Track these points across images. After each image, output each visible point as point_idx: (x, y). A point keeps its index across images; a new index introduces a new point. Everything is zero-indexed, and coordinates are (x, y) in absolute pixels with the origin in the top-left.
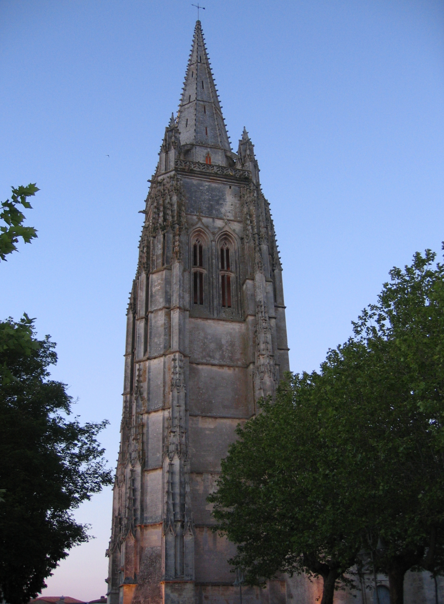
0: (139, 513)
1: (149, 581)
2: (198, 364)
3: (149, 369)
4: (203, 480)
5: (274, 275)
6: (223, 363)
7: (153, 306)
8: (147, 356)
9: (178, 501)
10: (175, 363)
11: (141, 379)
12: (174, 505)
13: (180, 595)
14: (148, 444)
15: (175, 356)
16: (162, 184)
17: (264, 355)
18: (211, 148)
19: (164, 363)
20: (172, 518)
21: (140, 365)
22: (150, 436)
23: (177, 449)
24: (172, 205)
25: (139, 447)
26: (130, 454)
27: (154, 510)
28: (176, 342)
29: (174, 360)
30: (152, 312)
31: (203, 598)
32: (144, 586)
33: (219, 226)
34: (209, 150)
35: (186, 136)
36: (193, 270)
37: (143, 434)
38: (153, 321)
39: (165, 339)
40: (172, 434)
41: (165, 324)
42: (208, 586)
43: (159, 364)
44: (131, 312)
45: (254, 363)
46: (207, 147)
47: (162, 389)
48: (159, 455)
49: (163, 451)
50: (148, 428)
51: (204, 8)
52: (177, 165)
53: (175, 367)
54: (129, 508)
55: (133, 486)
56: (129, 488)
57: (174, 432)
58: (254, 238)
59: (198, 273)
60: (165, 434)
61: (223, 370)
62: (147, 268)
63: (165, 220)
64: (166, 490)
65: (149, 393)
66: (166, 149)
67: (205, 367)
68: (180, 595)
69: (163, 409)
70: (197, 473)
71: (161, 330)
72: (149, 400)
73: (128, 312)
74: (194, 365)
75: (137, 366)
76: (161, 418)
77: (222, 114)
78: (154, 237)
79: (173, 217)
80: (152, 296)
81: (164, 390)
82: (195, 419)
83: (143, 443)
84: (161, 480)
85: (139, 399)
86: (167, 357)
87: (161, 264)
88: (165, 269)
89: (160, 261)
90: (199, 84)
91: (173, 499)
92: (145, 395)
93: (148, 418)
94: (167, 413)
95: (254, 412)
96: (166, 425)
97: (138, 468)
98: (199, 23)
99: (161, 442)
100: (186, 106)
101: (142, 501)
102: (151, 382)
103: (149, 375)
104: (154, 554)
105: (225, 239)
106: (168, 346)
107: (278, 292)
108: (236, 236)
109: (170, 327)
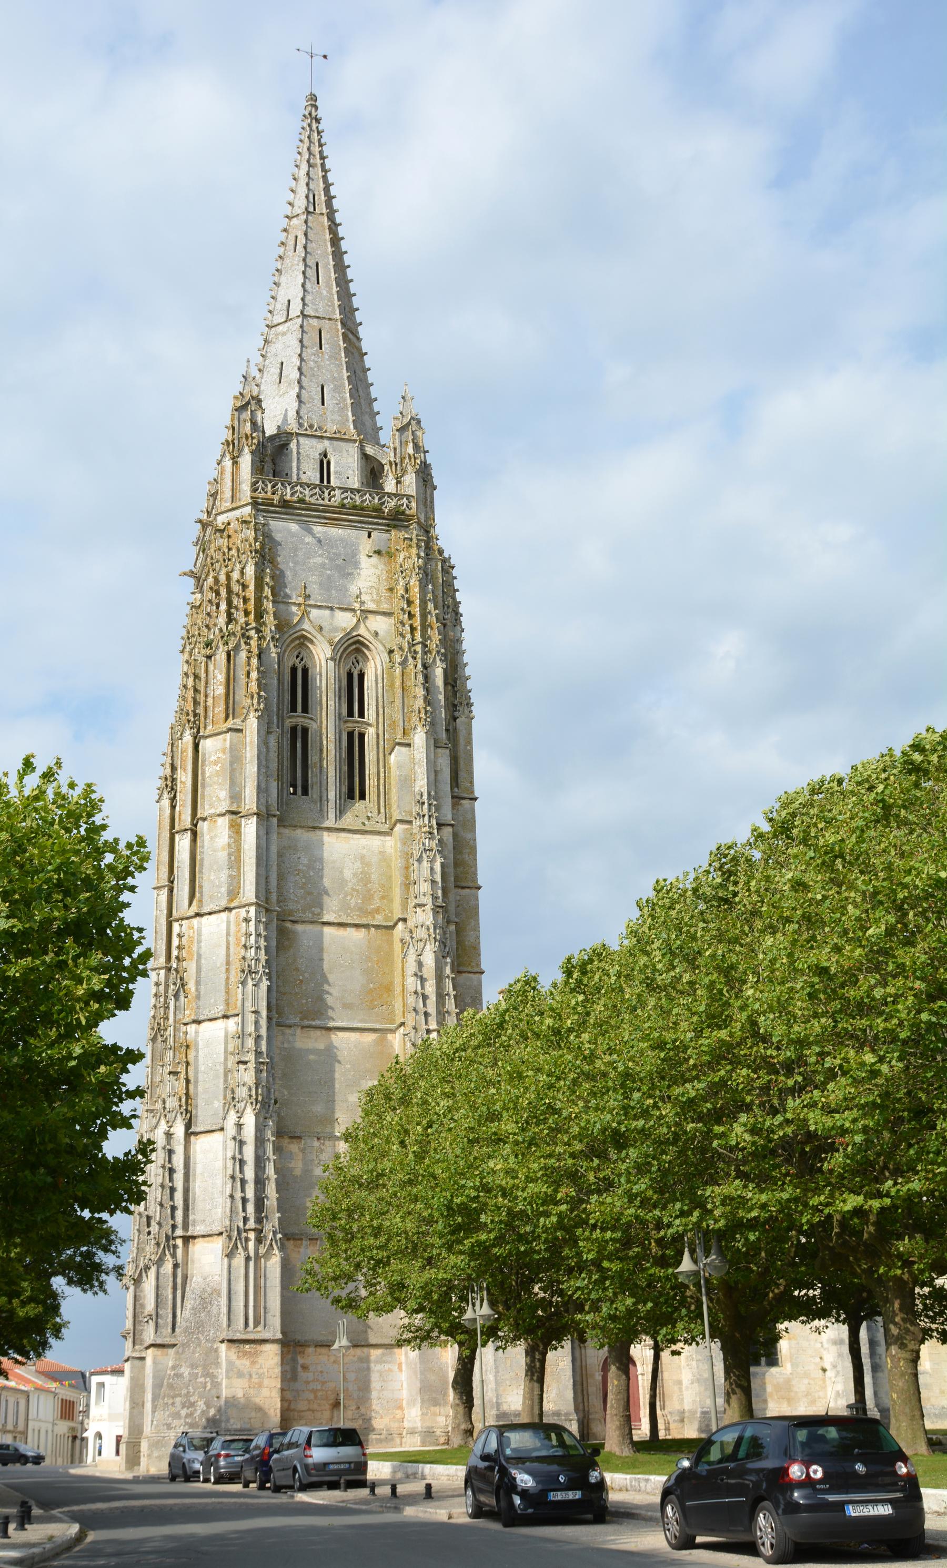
0: (179, 1214)
1: (198, 1338)
2: (294, 922)
3: (199, 935)
4: (303, 1150)
5: (455, 729)
6: (344, 920)
7: (207, 807)
8: (194, 909)
9: (250, 1193)
11: (184, 953)
12: (244, 1200)
13: (253, 1363)
14: (196, 1082)
15: (248, 912)
17: (424, 905)
18: (330, 439)
19: (228, 923)
20: (241, 1224)
22: (202, 1068)
23: (250, 1096)
24: (245, 587)
25: (180, 1086)
26: (164, 1102)
27: (208, 1207)
29: (247, 920)
30: (204, 819)
31: (300, 1369)
32: (189, 1346)
33: (344, 625)
34: (326, 443)
35: (277, 412)
36: (288, 723)
37: (188, 1064)
38: (207, 838)
39: (230, 876)
40: (242, 1067)
41: (229, 845)
42: (309, 1346)
43: (218, 925)
44: (166, 795)
46: (322, 437)
47: (224, 976)
48: (218, 1104)
49: (225, 1098)
50: (197, 1051)
51: (325, 57)
52: (255, 490)
54: (161, 1205)
55: (170, 1162)
56: (163, 1167)
57: (246, 1063)
58: (416, 652)
59: (299, 728)
60: (230, 1066)
62: (194, 722)
63: (230, 619)
64: (230, 1172)
65: (198, 983)
66: (233, 448)
68: (253, 1363)
69: (226, 1017)
70: (291, 1138)
71: (223, 855)
72: (198, 997)
73: (161, 796)
74: (288, 925)
75: (176, 927)
76: (222, 1034)
77: (359, 340)
78: (209, 657)
79: (247, 614)
81: (228, 978)
82: (288, 1031)
83: (188, 1081)
84: (221, 1153)
85: (182, 993)
86: (234, 912)
87: (223, 716)
88: (230, 730)
89: (220, 709)
90: (309, 271)
91: (243, 1190)
92: (191, 986)
93: (197, 1032)
94: (232, 1025)
95: (402, 1020)
96: (231, 1048)
97: (179, 1130)
98: (313, 98)
99: (222, 1080)
100: (281, 328)
101: (186, 1191)
103: (199, 948)
104: (209, 1290)
106: (233, 893)
108: (381, 647)
109: (239, 851)
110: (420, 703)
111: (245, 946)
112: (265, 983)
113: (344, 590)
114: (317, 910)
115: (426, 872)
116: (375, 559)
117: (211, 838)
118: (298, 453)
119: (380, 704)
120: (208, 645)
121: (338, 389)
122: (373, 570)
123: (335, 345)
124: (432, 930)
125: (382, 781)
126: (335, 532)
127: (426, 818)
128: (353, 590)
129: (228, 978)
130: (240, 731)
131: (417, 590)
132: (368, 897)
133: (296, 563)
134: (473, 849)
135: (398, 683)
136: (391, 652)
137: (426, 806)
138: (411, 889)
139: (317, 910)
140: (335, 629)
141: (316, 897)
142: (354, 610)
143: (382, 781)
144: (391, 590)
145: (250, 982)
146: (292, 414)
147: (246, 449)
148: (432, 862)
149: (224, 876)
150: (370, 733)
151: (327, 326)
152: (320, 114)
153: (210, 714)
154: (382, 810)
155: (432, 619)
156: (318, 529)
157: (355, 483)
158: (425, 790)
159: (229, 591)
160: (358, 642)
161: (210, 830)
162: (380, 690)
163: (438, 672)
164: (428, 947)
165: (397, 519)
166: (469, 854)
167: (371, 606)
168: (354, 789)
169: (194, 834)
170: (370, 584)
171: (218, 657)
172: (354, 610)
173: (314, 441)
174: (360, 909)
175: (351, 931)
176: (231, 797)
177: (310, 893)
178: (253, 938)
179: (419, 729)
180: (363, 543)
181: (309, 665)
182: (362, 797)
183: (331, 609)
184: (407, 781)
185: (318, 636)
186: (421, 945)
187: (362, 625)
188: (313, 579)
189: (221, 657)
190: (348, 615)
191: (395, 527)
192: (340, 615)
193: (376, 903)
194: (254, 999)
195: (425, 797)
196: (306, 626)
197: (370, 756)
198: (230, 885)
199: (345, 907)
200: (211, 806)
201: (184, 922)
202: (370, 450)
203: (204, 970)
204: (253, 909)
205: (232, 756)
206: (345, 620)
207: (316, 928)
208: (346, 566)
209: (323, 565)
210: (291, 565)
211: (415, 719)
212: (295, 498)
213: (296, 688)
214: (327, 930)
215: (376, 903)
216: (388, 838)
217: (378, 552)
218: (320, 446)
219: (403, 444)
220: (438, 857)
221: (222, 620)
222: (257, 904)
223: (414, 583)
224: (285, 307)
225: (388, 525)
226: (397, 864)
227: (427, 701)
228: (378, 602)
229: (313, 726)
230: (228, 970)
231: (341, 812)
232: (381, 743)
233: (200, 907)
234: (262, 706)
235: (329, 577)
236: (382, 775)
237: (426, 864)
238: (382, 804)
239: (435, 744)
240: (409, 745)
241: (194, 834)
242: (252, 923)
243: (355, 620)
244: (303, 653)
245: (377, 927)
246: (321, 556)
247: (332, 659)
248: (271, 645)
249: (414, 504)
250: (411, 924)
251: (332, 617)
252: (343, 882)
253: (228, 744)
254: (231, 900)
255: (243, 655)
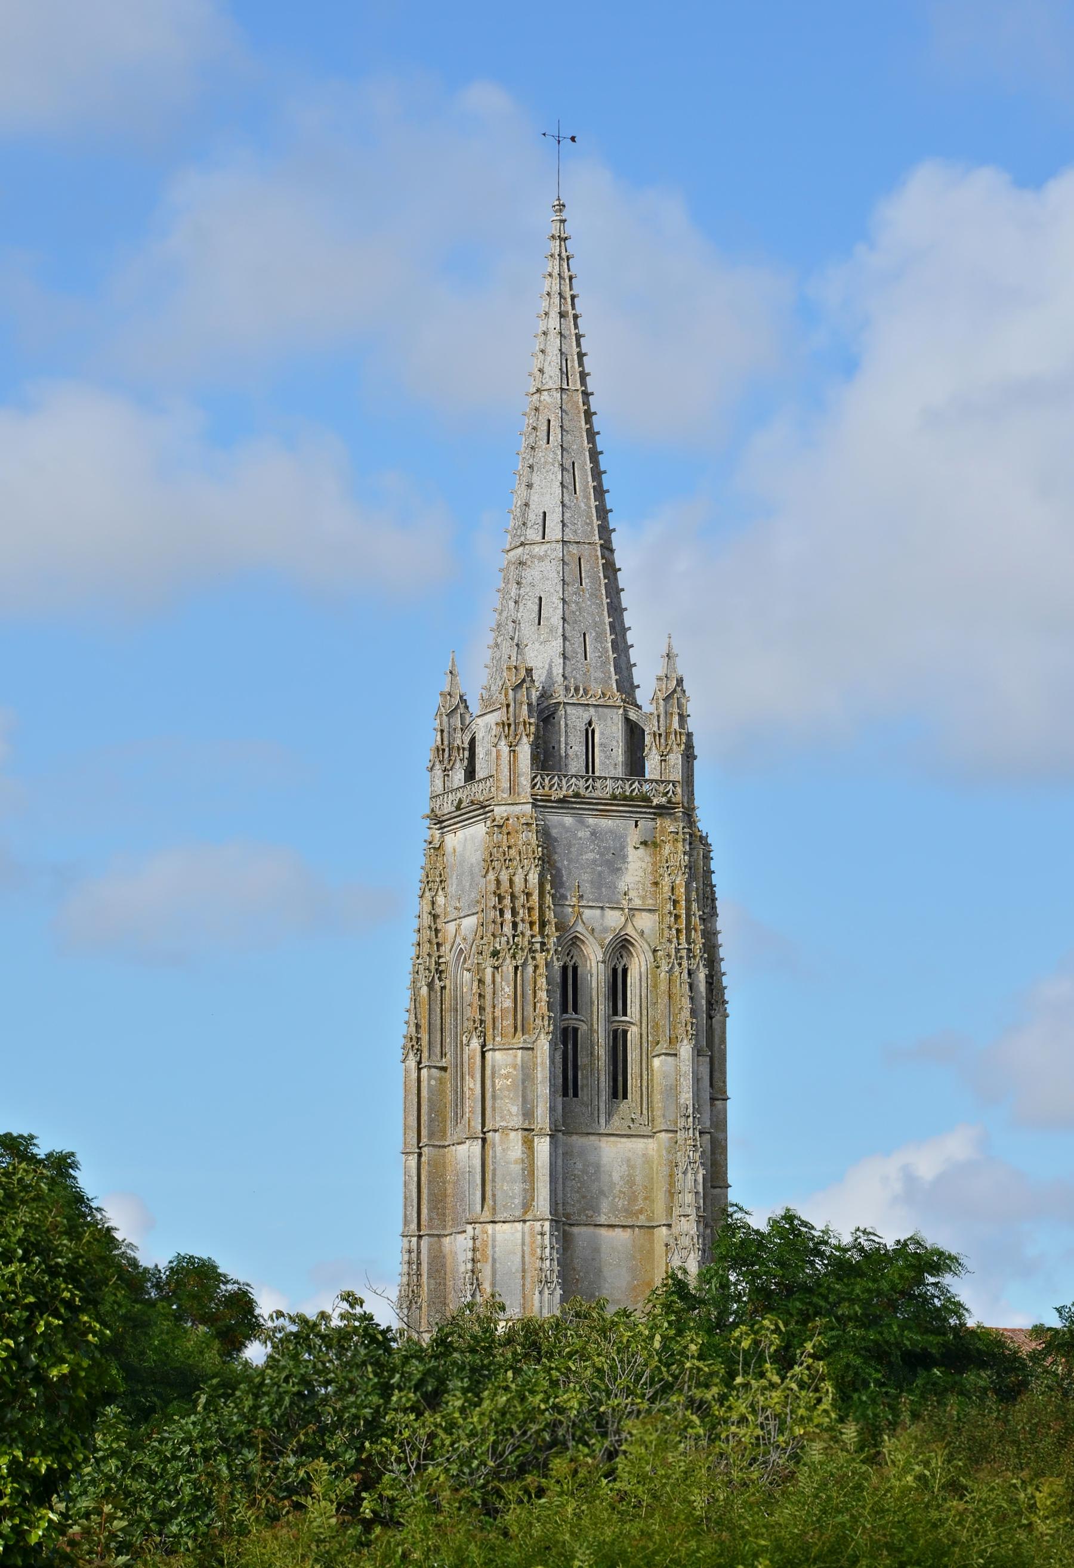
3: (494, 1240)
10: (543, 1239)
11: (478, 1255)
16: (505, 830)
19: (523, 1233)
21: (474, 1229)
28: (545, 1200)
33: (613, 924)
34: (592, 710)
38: (499, 1149)
43: (512, 1234)
45: (669, 1226)
53: (543, 1248)
61: (614, 1234)
67: (583, 1229)
71: (516, 1169)
74: (567, 1228)
80: (494, 1097)
81: (524, 1285)
85: (478, 1293)
86: (528, 1223)
102: (498, 1265)
105: (623, 946)
106: (527, 1205)
107: (716, 1066)
108: (646, 946)
110: (686, 1014)
111: (542, 1259)
112: (559, 1292)
113: (613, 887)
114: (590, 1213)
115: (690, 1184)
116: (642, 850)
117: (504, 1150)
118: (566, 725)
119: (644, 1005)
120: (495, 954)
121: (599, 638)
122: (639, 864)
123: (595, 579)
124: (695, 1240)
125: (645, 1084)
126: (605, 823)
127: (691, 1131)
128: (622, 886)
129: (524, 1285)
130: (533, 1049)
131: (683, 890)
132: (633, 1199)
133: (570, 861)
134: (725, 1148)
135: (663, 987)
136: (655, 951)
137: (691, 1119)
138: (676, 1197)
139: (590, 1213)
140: (605, 930)
141: (591, 1205)
142: (622, 909)
143: (645, 1084)
144: (656, 884)
145: (546, 1292)
146: (558, 670)
147: (525, 739)
148: (696, 1174)
149: (518, 1188)
150: (633, 1032)
151: (586, 553)
152: (569, 229)
153: (499, 1025)
154: (645, 1112)
155: (695, 920)
156: (591, 821)
157: (620, 772)
158: (690, 1103)
159: (513, 897)
160: (626, 940)
161: (502, 1142)
162: (644, 991)
163: (702, 975)
164: (692, 1255)
165: (663, 811)
166: (721, 1153)
167: (637, 903)
168: (618, 1090)
169: (484, 1140)
170: (637, 879)
171: (504, 968)
172: (622, 909)
173: (580, 709)
174: (626, 1210)
175: (618, 1230)
176: (524, 1115)
177: (584, 1197)
178: (547, 1250)
179: (685, 1042)
180: (631, 832)
181: (580, 963)
182: (625, 1097)
183: (602, 908)
184: (673, 1091)
185: (591, 938)
186: (685, 1253)
187: (630, 925)
188: (586, 877)
189: (508, 967)
190: (617, 913)
191: (660, 815)
192: (609, 913)
193: (640, 1204)
194: (549, 1307)
195: (690, 1110)
196: (580, 928)
197: (633, 1056)
198: (524, 1198)
199: (614, 1209)
200: (503, 1118)
201: (477, 1225)
202: (633, 715)
203: (499, 1273)
204: (547, 1224)
205: (524, 1074)
206: (614, 919)
207: (591, 1229)
208: (615, 861)
209: (594, 861)
210: (566, 863)
211: (681, 1030)
212: (570, 793)
213: (568, 986)
214: (603, 1231)
215: (640, 1204)
216: (650, 1140)
217: (644, 843)
218: (586, 715)
219: (668, 715)
220: (701, 1168)
221: (508, 929)
222: (552, 1220)
223: (680, 880)
224: (540, 521)
225: (654, 814)
226: (661, 1172)
227: (693, 1013)
228: (643, 898)
229: (583, 1028)
230: (523, 1277)
231: (609, 1115)
232: (645, 1045)
233: (494, 1213)
234: (551, 1028)
235: (600, 874)
236: (645, 1077)
237: (690, 1176)
238: (645, 1106)
239: (698, 1052)
240: (676, 1055)
241: (484, 1140)
242: (547, 1237)
243: (623, 919)
244: (574, 952)
245: (640, 1227)
246: (592, 851)
247: (603, 962)
248: (555, 958)
249: (679, 790)
250: (675, 1230)
251: (603, 916)
252: (612, 1185)
253: (519, 1060)
254: (525, 1213)
255: (530, 969)
